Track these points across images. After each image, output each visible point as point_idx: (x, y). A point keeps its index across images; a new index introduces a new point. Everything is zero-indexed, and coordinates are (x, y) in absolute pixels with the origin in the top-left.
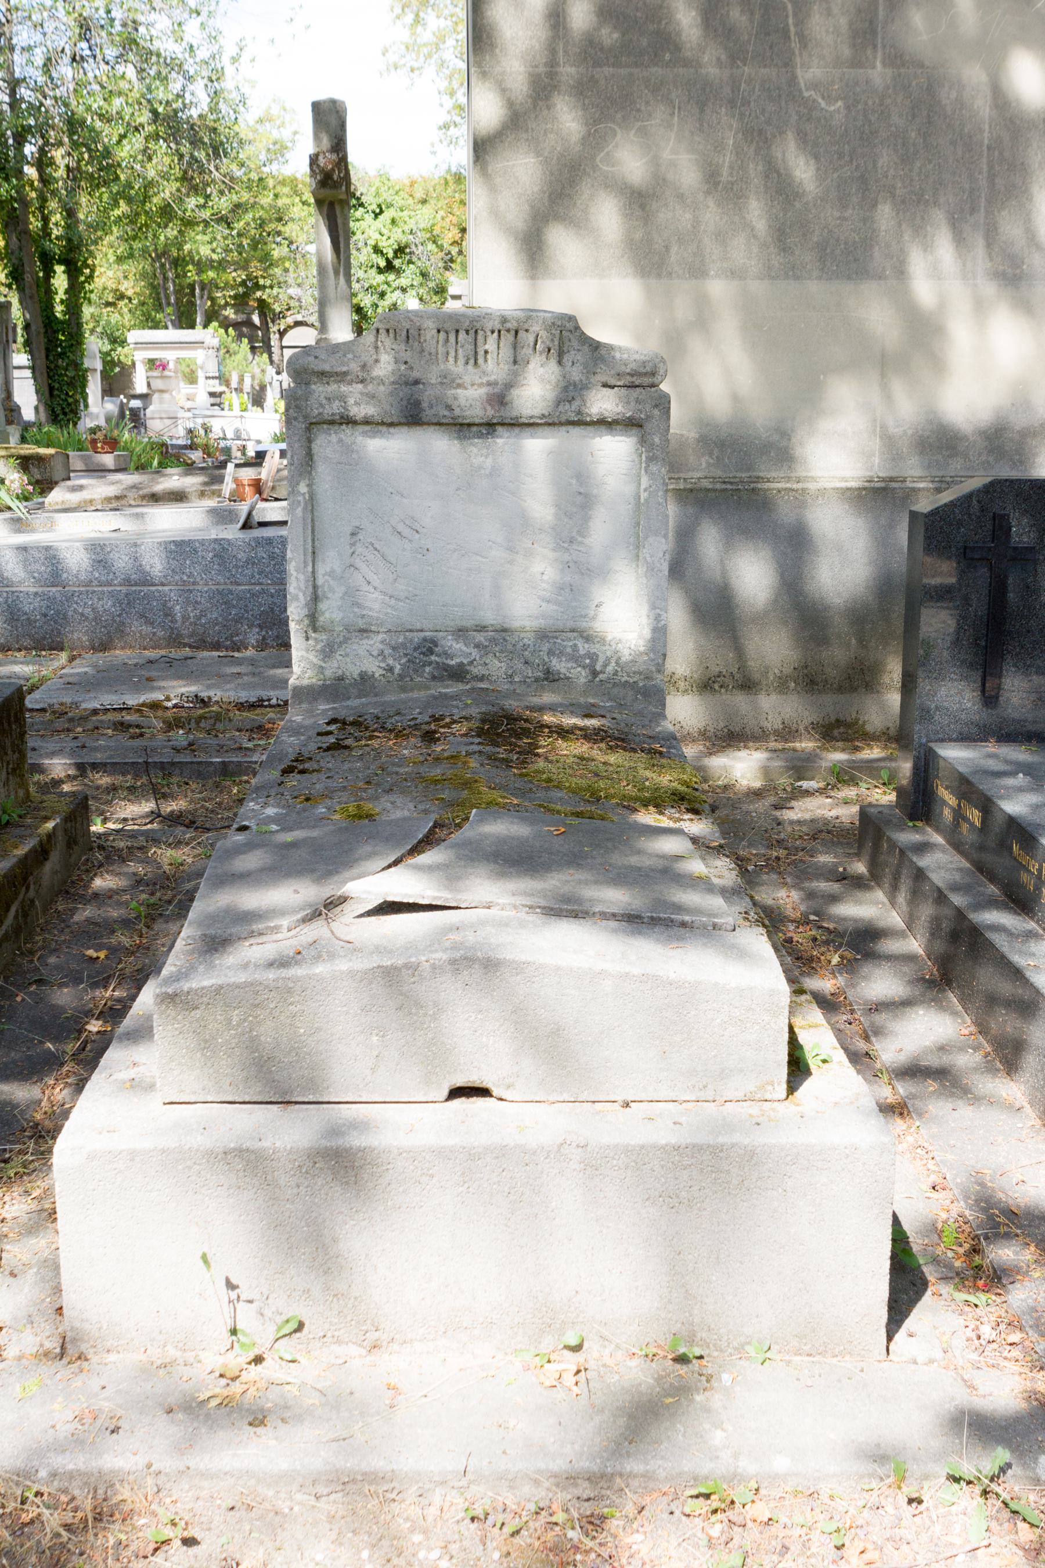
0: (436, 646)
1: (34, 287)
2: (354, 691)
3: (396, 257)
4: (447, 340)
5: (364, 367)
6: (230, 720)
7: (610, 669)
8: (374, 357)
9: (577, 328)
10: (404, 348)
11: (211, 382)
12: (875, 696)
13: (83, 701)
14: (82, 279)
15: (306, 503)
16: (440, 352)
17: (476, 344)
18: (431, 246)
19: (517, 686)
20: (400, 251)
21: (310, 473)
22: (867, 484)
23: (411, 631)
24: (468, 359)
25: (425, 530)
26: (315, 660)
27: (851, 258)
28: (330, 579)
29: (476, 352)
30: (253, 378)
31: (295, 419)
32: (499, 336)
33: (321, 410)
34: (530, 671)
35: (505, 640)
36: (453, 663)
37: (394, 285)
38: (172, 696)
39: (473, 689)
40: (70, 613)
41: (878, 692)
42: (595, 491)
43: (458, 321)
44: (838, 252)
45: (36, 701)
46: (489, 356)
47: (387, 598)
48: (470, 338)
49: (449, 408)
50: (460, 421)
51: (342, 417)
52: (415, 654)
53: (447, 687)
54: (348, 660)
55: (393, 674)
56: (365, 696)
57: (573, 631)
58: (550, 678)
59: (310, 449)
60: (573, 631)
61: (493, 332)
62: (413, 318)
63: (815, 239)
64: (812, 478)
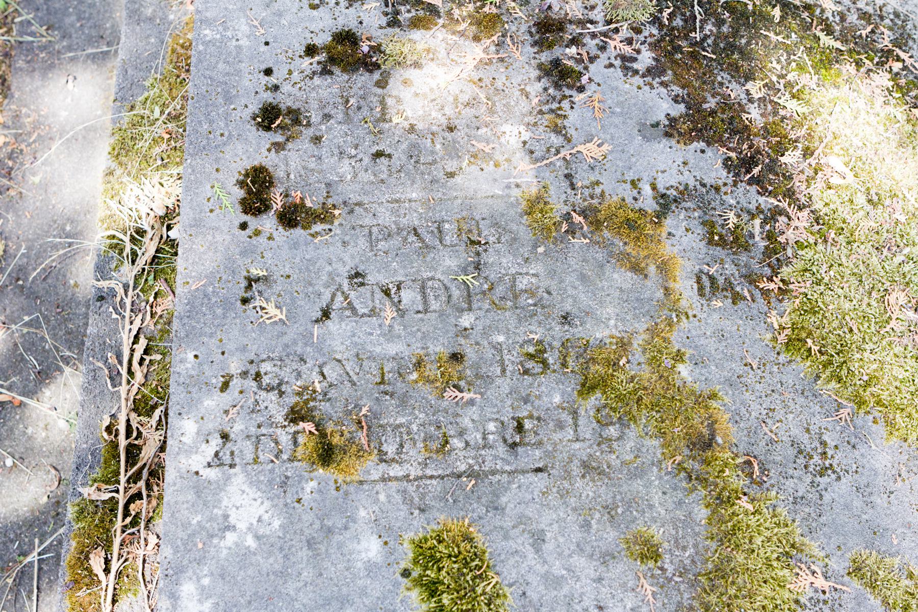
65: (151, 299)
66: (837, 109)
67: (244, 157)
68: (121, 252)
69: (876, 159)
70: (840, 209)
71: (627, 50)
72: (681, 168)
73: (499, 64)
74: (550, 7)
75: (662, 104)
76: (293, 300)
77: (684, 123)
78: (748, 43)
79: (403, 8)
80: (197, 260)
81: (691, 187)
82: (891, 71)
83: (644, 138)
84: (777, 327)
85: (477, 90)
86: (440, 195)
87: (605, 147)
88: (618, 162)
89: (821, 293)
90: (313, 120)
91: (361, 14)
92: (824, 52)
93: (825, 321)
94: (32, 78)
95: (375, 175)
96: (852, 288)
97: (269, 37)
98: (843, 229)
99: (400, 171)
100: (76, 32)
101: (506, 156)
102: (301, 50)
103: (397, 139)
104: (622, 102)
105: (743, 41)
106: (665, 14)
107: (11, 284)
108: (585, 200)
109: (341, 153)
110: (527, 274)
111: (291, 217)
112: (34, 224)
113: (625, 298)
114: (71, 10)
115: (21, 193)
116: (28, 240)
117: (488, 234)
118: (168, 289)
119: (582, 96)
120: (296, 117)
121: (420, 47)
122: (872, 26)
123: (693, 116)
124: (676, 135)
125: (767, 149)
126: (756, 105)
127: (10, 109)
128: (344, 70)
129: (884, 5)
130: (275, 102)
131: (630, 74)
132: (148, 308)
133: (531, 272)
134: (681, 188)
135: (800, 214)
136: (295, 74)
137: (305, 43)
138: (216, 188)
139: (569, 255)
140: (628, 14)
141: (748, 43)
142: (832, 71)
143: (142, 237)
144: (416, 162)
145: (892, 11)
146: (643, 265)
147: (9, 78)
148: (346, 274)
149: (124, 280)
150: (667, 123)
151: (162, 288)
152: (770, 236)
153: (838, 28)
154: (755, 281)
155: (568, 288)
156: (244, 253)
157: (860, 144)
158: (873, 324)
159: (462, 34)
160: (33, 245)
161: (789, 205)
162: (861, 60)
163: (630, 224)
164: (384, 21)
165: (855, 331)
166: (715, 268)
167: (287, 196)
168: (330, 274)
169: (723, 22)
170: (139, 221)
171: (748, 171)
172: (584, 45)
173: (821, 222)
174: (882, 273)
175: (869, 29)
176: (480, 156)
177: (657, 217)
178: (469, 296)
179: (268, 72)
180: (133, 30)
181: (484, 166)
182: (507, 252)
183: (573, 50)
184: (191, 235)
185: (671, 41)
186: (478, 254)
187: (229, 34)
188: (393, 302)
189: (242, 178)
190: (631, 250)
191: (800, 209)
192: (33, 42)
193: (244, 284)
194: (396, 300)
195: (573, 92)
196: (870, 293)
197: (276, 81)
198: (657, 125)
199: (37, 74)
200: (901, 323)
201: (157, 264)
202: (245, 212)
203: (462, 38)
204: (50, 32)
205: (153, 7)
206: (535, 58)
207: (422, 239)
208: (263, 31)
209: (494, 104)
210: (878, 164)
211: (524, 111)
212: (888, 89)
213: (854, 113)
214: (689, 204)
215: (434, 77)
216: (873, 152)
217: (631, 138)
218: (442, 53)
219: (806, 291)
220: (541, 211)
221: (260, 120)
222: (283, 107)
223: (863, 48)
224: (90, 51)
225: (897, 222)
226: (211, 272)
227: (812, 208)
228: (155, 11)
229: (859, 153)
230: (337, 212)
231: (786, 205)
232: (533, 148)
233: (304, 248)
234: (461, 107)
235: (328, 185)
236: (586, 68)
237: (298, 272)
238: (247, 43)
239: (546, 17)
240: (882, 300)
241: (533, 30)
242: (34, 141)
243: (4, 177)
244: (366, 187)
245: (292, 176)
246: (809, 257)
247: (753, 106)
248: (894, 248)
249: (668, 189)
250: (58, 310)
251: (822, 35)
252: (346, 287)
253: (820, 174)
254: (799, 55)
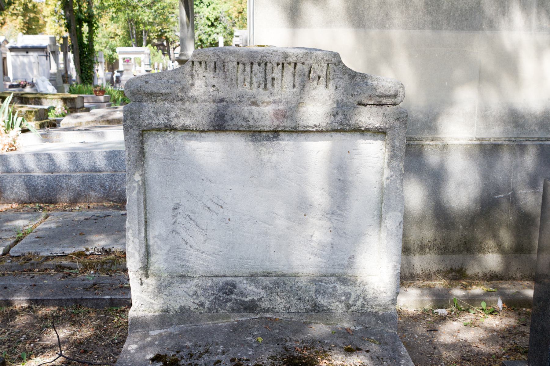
0: (235, 288)
1: (75, 32)
2: (176, 320)
3: (215, 21)
4: (244, 70)
5: (183, 89)
6: (120, 264)
7: (359, 303)
8: (190, 82)
9: (340, 62)
10: (212, 76)
11: (147, 66)
12: (472, 256)
13: (41, 252)
14: (94, 28)
15: (140, 189)
16: (239, 78)
17: (265, 73)
18: (228, 18)
19: (292, 316)
20: (216, 19)
21: (143, 166)
22: (470, 142)
23: (217, 276)
24: (260, 84)
25: (227, 206)
26: (147, 299)
27: (464, 18)
28: (158, 240)
29: (265, 79)
30: (163, 65)
31: (131, 127)
32: (283, 67)
33: (150, 121)
34: (302, 305)
35: (284, 283)
36: (247, 299)
37: (214, 32)
38: (90, 248)
39: (260, 318)
40: (55, 186)
41: (473, 253)
42: (350, 179)
43: (253, 56)
44: (457, 15)
45: (15, 252)
46: (275, 82)
47: (200, 253)
48: (262, 68)
49: (246, 120)
50: (254, 129)
51: (166, 126)
52: (220, 294)
53: (242, 316)
54: (171, 298)
55: (204, 308)
56: (184, 323)
57: (332, 275)
58: (317, 310)
59: (143, 148)
60: (332, 275)
61: (278, 64)
62: (219, 53)
63: (445, 8)
64: (440, 138)
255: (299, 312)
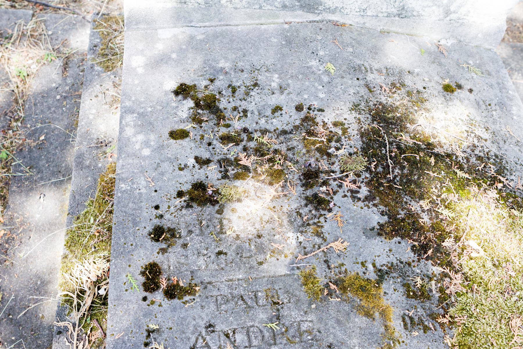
2: (197, 16)
65: (89, 332)
66: (471, 212)
67: (144, 258)
68: (72, 303)
69: (494, 240)
70: (478, 271)
71: (354, 187)
72: (388, 253)
73: (284, 198)
74: (310, 165)
75: (375, 217)
76: (174, 342)
77: (388, 227)
78: (419, 178)
79: (230, 168)
80: (118, 320)
81: (395, 264)
82: (497, 189)
83: (366, 237)
84: (450, 345)
85: (273, 213)
86: (255, 276)
87: (346, 244)
88: (353, 252)
89: (473, 323)
90: (182, 234)
91: (207, 172)
92: (460, 181)
93: (477, 340)
94: (21, 196)
95: (218, 265)
96: (490, 318)
97: (157, 187)
98: (481, 283)
99: (232, 262)
100: (45, 169)
101: (291, 251)
102: (175, 194)
103: (229, 243)
104: (353, 217)
105: (416, 177)
106: (372, 165)
107: (5, 317)
108: (336, 275)
109: (199, 253)
110: (306, 321)
111: (172, 292)
112: (20, 281)
113: (363, 333)
114: (43, 157)
115: (12, 263)
116: (16, 291)
117: (283, 298)
118: (99, 325)
119: (331, 214)
120: (173, 232)
121: (240, 190)
122: (484, 164)
123: (392, 222)
124: (384, 234)
125: (434, 239)
126: (426, 213)
127: (8, 214)
128: (199, 205)
129: (489, 151)
130: (161, 225)
131: (356, 200)
132: (87, 338)
133: (309, 319)
134: (389, 265)
135: (456, 276)
136: (172, 208)
137: (177, 190)
138: (129, 277)
139: (330, 308)
140: (353, 167)
141: (419, 178)
142: (466, 191)
143: (83, 294)
144: (241, 257)
145: (493, 154)
146: (371, 312)
147: (8, 196)
148: (204, 326)
149: (73, 321)
150: (379, 228)
151: (95, 325)
152: (442, 290)
153: (466, 166)
154: (435, 318)
155: (330, 328)
156: (145, 315)
157: (485, 232)
158: (504, 340)
159: (263, 181)
160: (19, 294)
161: (450, 271)
162: (480, 183)
163: (363, 288)
164: (220, 176)
165: (495, 344)
166: (412, 312)
167: (169, 280)
168: (195, 326)
169: (404, 167)
170: (82, 285)
171: (426, 253)
172: (330, 185)
173: (469, 279)
174: (506, 308)
175: (483, 166)
176: (276, 251)
177: (378, 284)
178: (274, 335)
179: (157, 207)
180: (79, 174)
181: (279, 257)
182: (294, 308)
183: (324, 189)
184: (115, 305)
185: (377, 180)
186: (278, 310)
187: (135, 186)
188: (231, 341)
189: (143, 270)
190: (364, 304)
191: (456, 273)
192: (21, 176)
193: (146, 334)
194: (233, 340)
195: (326, 212)
196: (501, 320)
197: (161, 213)
198: (373, 229)
199: (23, 194)
200: (520, 338)
201: (92, 310)
202: (146, 290)
203: (263, 184)
204: (31, 170)
205: (90, 160)
206: (303, 194)
207: (245, 302)
208: (153, 184)
209: (282, 221)
210: (496, 243)
211: (299, 224)
212: (496, 199)
213: (480, 214)
214: (394, 275)
215: (248, 207)
216: (493, 236)
217: (359, 237)
218: (252, 193)
219: (464, 322)
220: (312, 283)
221: (153, 236)
222: (165, 227)
223: (481, 176)
224: (53, 181)
225: (511, 276)
226: (127, 328)
227: (463, 272)
228: (91, 162)
229: (485, 237)
230: (197, 288)
231: (448, 271)
232: (305, 246)
233: (179, 310)
234: (264, 223)
235: (192, 272)
236: (332, 198)
237: (176, 325)
238: (145, 191)
239: (308, 170)
240: (507, 324)
241: (302, 178)
242: (21, 232)
243: (3, 254)
244: (214, 273)
245: (172, 268)
246: (464, 301)
247: (424, 214)
248: (511, 292)
249: (382, 266)
250: (32, 333)
251: (458, 171)
252: (204, 333)
253: (465, 252)
254: (447, 183)
255: (377, 16)
